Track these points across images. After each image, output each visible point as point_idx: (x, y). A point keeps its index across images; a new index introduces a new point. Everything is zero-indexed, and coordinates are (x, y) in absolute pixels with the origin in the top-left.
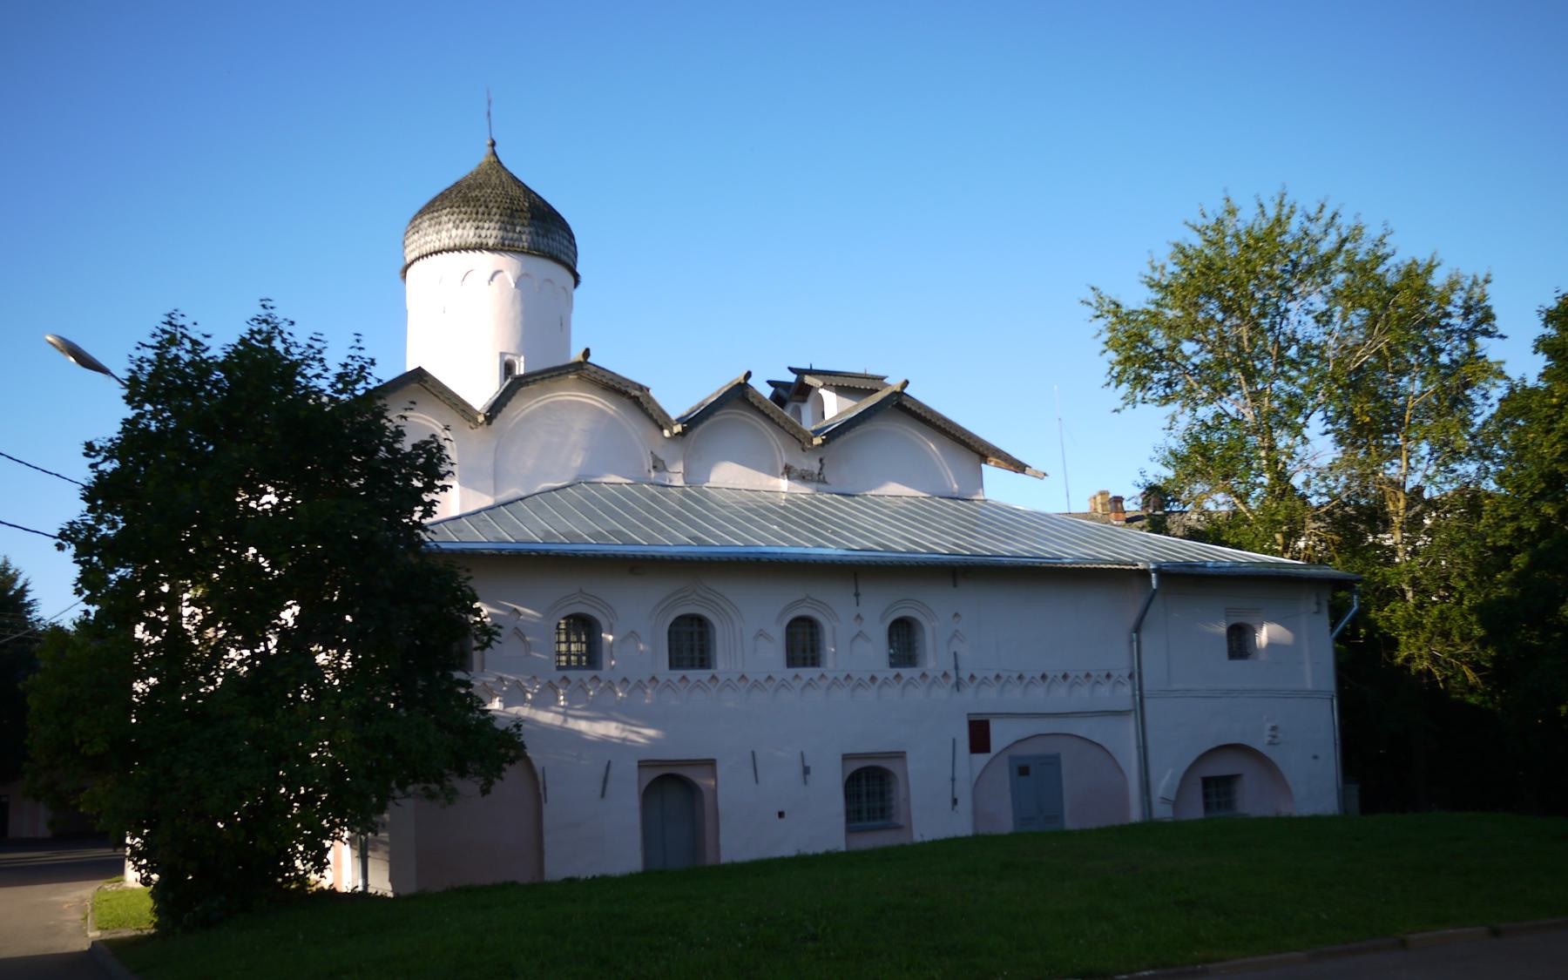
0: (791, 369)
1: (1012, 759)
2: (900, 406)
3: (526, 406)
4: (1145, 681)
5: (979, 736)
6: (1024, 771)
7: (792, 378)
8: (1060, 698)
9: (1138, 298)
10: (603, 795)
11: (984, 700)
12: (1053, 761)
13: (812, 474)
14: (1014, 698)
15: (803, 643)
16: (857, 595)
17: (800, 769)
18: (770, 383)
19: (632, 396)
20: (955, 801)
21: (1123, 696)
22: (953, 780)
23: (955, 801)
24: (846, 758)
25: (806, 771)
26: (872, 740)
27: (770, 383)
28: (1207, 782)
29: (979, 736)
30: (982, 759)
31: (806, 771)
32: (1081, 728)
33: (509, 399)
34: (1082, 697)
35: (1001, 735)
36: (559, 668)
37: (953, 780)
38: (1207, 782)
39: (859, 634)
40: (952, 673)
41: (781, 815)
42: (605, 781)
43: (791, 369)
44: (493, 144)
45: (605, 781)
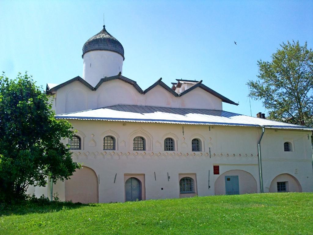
0: (176, 80)
2: (200, 85)
3: (104, 86)
4: (262, 157)
5: (216, 170)
6: (228, 179)
7: (177, 82)
9: (270, 60)
10: (114, 183)
12: (237, 177)
13: (212, 128)
17: (167, 177)
18: (172, 83)
19: (134, 84)
20: (209, 187)
23: (209, 187)
25: (169, 177)
26: (187, 171)
27: (172, 83)
28: (278, 183)
29: (216, 170)
30: (217, 176)
31: (169, 177)
33: (101, 84)
36: (104, 149)
37: (209, 181)
38: (278, 183)
41: (162, 189)
42: (115, 179)
43: (176, 80)
45: (115, 179)
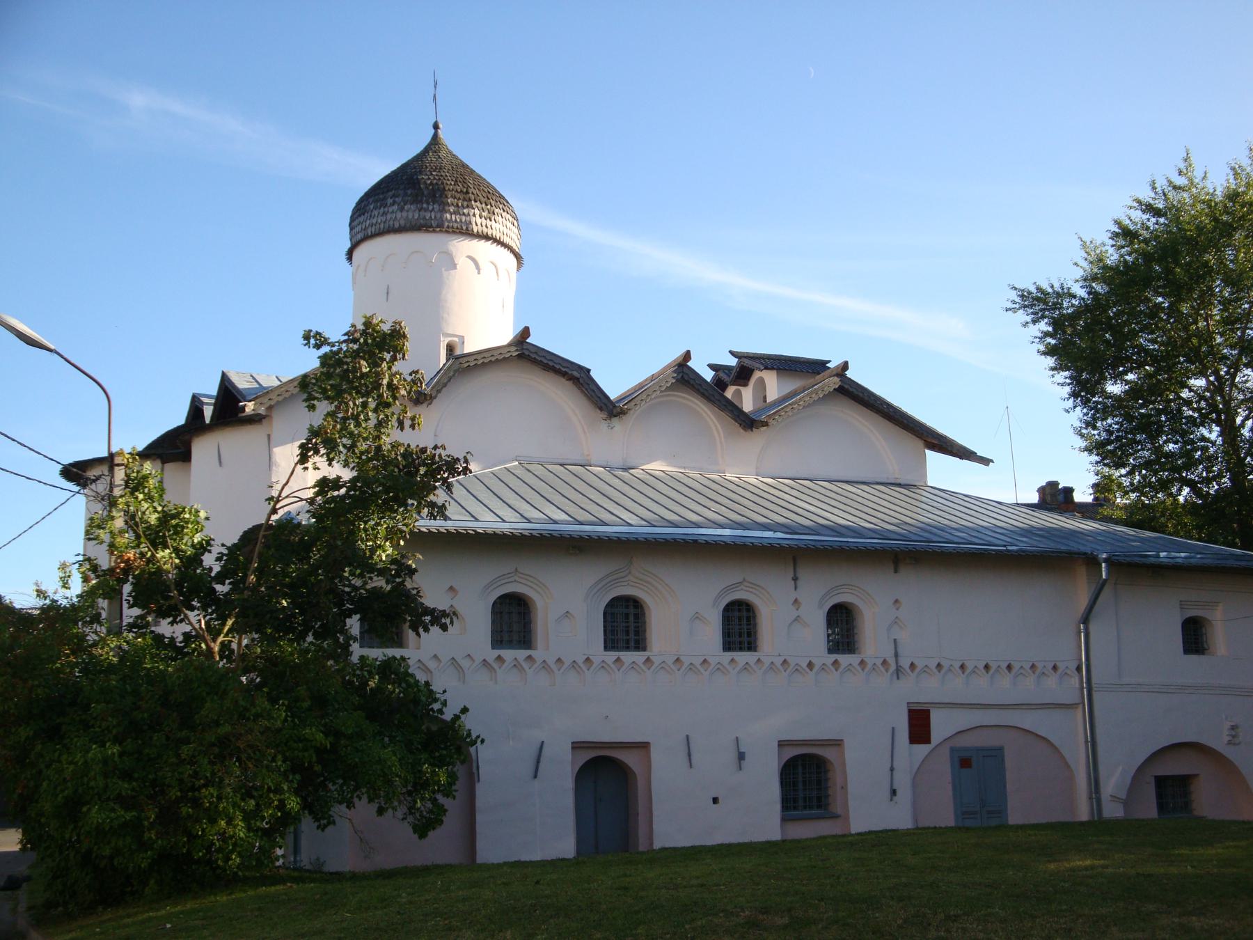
1: (953, 750)
6: (965, 763)
8: (1004, 688)
11: (925, 690)
14: (956, 687)
15: (740, 627)
16: (795, 579)
21: (1068, 689)
22: (892, 769)
24: (782, 744)
30: (922, 750)
32: (1027, 720)
34: (1027, 689)
35: (940, 726)
37: (892, 769)
39: (797, 619)
40: (892, 661)
44: (436, 127)
